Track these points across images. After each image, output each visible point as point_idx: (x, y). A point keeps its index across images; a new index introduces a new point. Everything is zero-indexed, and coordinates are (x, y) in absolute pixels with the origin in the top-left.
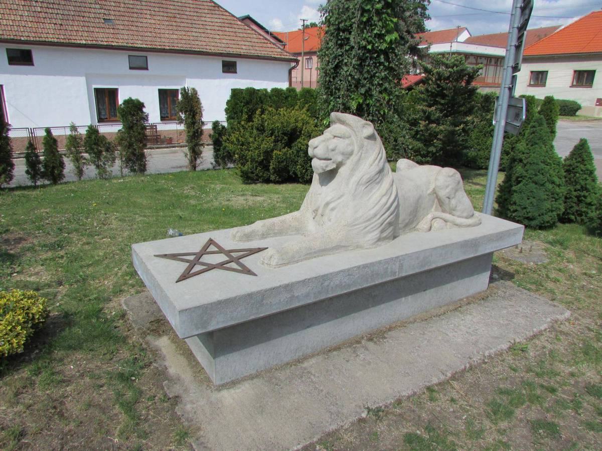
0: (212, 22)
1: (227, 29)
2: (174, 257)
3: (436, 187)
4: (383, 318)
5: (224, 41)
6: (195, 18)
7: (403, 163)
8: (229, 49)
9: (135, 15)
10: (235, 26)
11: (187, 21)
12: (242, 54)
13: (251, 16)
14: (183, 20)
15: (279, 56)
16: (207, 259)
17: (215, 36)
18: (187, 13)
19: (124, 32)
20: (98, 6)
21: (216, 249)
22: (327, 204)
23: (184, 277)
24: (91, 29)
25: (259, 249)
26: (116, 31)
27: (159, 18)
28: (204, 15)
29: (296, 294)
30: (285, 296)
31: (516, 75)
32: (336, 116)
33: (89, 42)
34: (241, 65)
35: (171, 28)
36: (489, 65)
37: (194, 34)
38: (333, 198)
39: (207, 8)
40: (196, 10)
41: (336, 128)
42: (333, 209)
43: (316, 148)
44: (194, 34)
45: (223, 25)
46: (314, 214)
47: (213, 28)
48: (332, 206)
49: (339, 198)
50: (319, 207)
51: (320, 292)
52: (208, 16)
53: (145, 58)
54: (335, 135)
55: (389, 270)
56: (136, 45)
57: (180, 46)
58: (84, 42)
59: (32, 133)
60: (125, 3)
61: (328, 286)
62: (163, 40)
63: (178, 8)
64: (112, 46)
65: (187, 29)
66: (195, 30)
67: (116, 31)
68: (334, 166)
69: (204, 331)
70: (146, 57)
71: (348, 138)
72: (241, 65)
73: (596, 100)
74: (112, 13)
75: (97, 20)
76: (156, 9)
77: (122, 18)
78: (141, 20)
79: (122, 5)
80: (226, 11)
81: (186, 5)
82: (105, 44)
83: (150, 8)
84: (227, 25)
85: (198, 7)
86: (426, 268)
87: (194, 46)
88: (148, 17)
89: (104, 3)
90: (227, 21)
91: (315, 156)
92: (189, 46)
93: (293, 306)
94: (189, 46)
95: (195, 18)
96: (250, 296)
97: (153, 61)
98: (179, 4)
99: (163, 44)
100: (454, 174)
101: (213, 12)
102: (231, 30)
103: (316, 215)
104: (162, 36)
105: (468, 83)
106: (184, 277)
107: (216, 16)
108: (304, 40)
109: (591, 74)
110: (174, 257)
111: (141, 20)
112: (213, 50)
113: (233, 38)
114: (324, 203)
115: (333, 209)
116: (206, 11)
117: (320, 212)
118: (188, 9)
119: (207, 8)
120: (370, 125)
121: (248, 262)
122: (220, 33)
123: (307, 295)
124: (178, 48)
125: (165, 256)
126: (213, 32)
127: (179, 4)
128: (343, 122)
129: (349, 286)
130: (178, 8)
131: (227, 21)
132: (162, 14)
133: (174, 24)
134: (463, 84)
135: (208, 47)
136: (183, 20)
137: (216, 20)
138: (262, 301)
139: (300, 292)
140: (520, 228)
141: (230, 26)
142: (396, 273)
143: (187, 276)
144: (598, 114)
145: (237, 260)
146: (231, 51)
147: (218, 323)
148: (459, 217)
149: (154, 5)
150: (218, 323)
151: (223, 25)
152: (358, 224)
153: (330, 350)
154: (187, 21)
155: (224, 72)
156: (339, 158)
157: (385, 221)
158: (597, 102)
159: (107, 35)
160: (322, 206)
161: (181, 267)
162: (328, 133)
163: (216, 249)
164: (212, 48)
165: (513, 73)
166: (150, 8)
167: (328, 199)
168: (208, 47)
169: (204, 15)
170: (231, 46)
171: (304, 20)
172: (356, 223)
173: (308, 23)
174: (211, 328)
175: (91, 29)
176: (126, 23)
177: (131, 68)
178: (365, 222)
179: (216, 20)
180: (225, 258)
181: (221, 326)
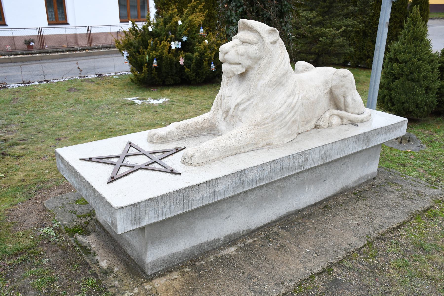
2: (100, 160)
4: (290, 207)
7: (301, 64)
16: (130, 161)
21: (137, 152)
22: (237, 105)
23: (113, 179)
29: (217, 189)
30: (208, 191)
31: (123, 19)
32: (244, 23)
38: (243, 100)
41: (242, 35)
42: (243, 110)
43: (227, 53)
46: (225, 116)
49: (249, 100)
50: (229, 109)
51: (238, 187)
54: (244, 41)
59: (40, 32)
68: (244, 70)
69: (138, 226)
71: (256, 43)
91: (225, 61)
96: (177, 192)
100: (349, 74)
103: (227, 116)
106: (113, 179)
110: (100, 160)
115: (243, 110)
117: (231, 112)
120: (275, 31)
121: (170, 162)
123: (227, 189)
125: (90, 159)
128: (250, 29)
139: (251, 175)
143: (116, 177)
148: (353, 113)
150: (150, 219)
152: (267, 123)
156: (247, 63)
157: (290, 119)
161: (108, 170)
162: (235, 40)
163: (137, 152)
167: (239, 100)
172: (266, 122)
174: (144, 224)
180: (147, 160)
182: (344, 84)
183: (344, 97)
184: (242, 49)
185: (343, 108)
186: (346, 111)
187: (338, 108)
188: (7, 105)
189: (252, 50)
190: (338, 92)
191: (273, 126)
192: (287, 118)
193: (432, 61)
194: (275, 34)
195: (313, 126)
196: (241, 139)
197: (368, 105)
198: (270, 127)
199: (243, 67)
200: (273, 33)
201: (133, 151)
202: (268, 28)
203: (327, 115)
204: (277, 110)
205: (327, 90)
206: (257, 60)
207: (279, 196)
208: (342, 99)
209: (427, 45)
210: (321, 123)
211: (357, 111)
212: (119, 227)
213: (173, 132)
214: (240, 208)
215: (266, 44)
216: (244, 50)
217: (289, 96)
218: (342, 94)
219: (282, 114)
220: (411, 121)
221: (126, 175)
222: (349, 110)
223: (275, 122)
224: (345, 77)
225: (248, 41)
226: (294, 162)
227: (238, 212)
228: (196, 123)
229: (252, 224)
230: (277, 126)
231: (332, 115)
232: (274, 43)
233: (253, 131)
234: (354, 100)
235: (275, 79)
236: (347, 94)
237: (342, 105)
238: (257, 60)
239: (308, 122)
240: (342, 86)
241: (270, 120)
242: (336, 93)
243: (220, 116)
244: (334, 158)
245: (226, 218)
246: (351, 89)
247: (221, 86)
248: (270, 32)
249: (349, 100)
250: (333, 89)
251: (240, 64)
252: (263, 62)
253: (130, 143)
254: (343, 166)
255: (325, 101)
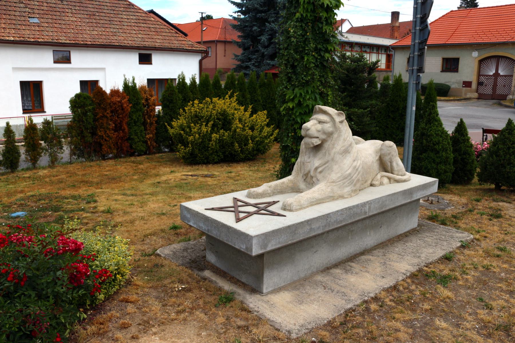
0: (128, 19)
1: (143, 25)
3: (381, 155)
5: (140, 36)
6: (112, 15)
8: (145, 43)
9: (58, 14)
10: (149, 22)
11: (105, 18)
12: (157, 46)
13: (154, 10)
14: (102, 18)
15: (190, 48)
17: (131, 32)
18: (105, 11)
19: (47, 29)
20: (22, 5)
22: (316, 169)
24: (19, 27)
25: (274, 202)
26: (42, 29)
27: (79, 16)
28: (121, 13)
32: (319, 108)
33: (17, 39)
34: (156, 58)
35: (91, 24)
36: (372, 53)
37: (112, 30)
39: (123, 6)
40: (113, 8)
42: (321, 172)
44: (112, 30)
45: (139, 21)
47: (129, 24)
48: (320, 170)
49: (325, 164)
50: (309, 172)
51: (325, 226)
52: (124, 13)
53: (68, 52)
55: (363, 211)
56: (61, 41)
57: (100, 41)
58: (12, 39)
60: (47, 3)
61: (330, 221)
62: (85, 36)
63: (97, 7)
64: (39, 42)
65: (106, 26)
66: (113, 26)
67: (42, 29)
70: (70, 52)
72: (156, 58)
73: (462, 82)
74: (36, 11)
75: (23, 19)
76: (77, 8)
77: (46, 17)
78: (63, 18)
79: (45, 4)
80: (140, 9)
81: (104, 4)
82: (32, 40)
83: (71, 7)
84: (142, 22)
85: (114, 5)
86: (384, 209)
87: (113, 41)
88: (70, 15)
89: (28, 2)
90: (141, 18)
92: (109, 41)
93: (311, 235)
94: (109, 41)
95: (112, 15)
97: (76, 57)
98: (97, 3)
99: (86, 39)
100: (393, 145)
101: (129, 10)
102: (145, 25)
104: (84, 32)
105: (370, 73)
107: (131, 14)
108: (202, 31)
109: (456, 61)
111: (63, 18)
112: (133, 44)
113: (148, 33)
114: (313, 168)
115: (321, 172)
116: (122, 9)
118: (106, 8)
119: (123, 6)
120: (342, 114)
122: (136, 28)
124: (99, 43)
126: (129, 28)
127: (97, 3)
129: (341, 221)
130: (97, 7)
131: (141, 18)
132: (82, 12)
133: (94, 21)
134: (366, 75)
135: (125, 42)
136: (102, 18)
137: (132, 17)
138: (295, 231)
140: (436, 181)
141: (144, 22)
142: (366, 212)
144: (466, 94)
145: (260, 209)
146: (147, 44)
147: (272, 245)
149: (74, 4)
151: (139, 21)
153: (327, 269)
154: (105, 18)
155: (140, 63)
156: (323, 137)
158: (463, 84)
159: (33, 32)
160: (313, 170)
164: (130, 42)
165: (418, 73)
166: (71, 7)
168: (125, 42)
169: (121, 13)
170: (147, 40)
171: (202, 13)
173: (204, 15)
175: (19, 27)
176: (50, 21)
177: (55, 62)
178: (343, 179)
179: (132, 17)
181: (274, 248)
182: (391, 152)
183: (391, 162)
184: (319, 127)
185: (390, 171)
186: (392, 173)
187: (386, 171)
188: (85, 172)
189: (328, 127)
190: (387, 159)
191: (344, 183)
192: (354, 177)
193: (198, 335)
194: (342, 116)
195: (369, 185)
196: (323, 192)
197: (407, 171)
198: (342, 184)
199: (320, 140)
200: (341, 115)
201: (240, 203)
202: (336, 111)
203: (379, 176)
204: (347, 171)
205: (377, 158)
206: (330, 135)
207: (350, 238)
208: (389, 164)
209: (446, 133)
210: (374, 182)
211: (400, 173)
212: (254, 250)
213: (267, 190)
214: (324, 245)
215: (336, 123)
216: (320, 127)
217: (354, 161)
218: (389, 160)
219: (350, 174)
220: (441, 185)
221: (246, 218)
222: (396, 172)
223: (345, 181)
224: (391, 147)
225: (323, 121)
226: (362, 209)
227: (323, 248)
228: (283, 183)
229: (332, 259)
230: (346, 183)
231: (382, 177)
232: (341, 122)
233: (330, 187)
234: (397, 164)
235: (344, 148)
236: (393, 160)
237: (389, 169)
238: (330, 135)
239: (366, 182)
240: (389, 154)
241: (341, 178)
242: (384, 159)
243: (300, 178)
244: (388, 208)
245: (315, 252)
246: (395, 157)
247: (300, 155)
248: (339, 115)
249: (394, 164)
250: (382, 157)
251: (318, 138)
252: (335, 136)
253: (236, 198)
254: (393, 216)
255: (376, 166)
